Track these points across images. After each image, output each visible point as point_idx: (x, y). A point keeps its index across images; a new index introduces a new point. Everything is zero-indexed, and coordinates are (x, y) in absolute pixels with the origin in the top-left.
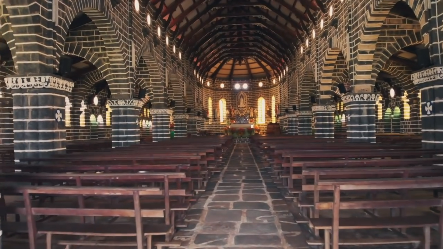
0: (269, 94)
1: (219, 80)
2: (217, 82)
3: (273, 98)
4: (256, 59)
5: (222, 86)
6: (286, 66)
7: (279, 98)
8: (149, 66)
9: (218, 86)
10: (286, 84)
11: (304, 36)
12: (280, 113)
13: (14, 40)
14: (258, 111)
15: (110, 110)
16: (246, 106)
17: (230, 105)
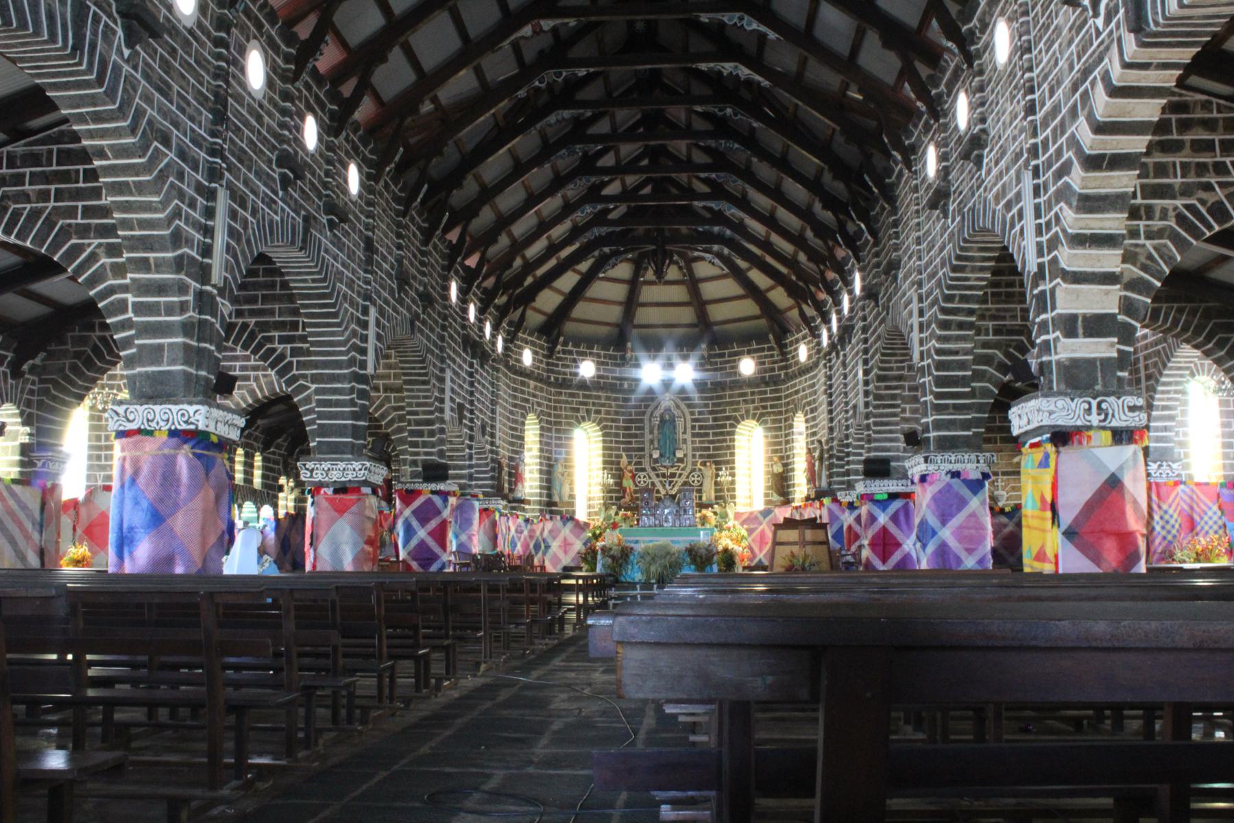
0: (781, 406)
1: (576, 345)
2: (564, 352)
3: (800, 423)
4: (727, 261)
5: (587, 369)
6: (851, 272)
7: (823, 417)
8: (101, 154)
9: (568, 370)
10: (852, 349)
11: (942, 87)
12: (830, 484)
13: (133, 332)
14: (736, 478)
15: (23, 434)
16: (685, 455)
17: (618, 449)
